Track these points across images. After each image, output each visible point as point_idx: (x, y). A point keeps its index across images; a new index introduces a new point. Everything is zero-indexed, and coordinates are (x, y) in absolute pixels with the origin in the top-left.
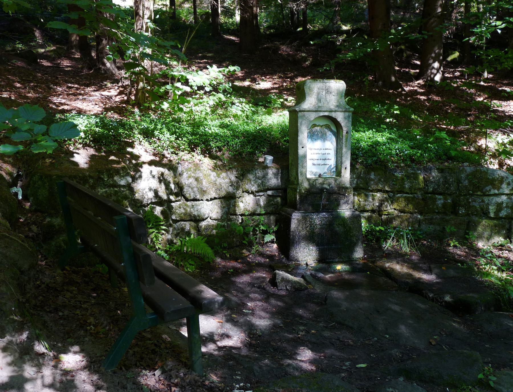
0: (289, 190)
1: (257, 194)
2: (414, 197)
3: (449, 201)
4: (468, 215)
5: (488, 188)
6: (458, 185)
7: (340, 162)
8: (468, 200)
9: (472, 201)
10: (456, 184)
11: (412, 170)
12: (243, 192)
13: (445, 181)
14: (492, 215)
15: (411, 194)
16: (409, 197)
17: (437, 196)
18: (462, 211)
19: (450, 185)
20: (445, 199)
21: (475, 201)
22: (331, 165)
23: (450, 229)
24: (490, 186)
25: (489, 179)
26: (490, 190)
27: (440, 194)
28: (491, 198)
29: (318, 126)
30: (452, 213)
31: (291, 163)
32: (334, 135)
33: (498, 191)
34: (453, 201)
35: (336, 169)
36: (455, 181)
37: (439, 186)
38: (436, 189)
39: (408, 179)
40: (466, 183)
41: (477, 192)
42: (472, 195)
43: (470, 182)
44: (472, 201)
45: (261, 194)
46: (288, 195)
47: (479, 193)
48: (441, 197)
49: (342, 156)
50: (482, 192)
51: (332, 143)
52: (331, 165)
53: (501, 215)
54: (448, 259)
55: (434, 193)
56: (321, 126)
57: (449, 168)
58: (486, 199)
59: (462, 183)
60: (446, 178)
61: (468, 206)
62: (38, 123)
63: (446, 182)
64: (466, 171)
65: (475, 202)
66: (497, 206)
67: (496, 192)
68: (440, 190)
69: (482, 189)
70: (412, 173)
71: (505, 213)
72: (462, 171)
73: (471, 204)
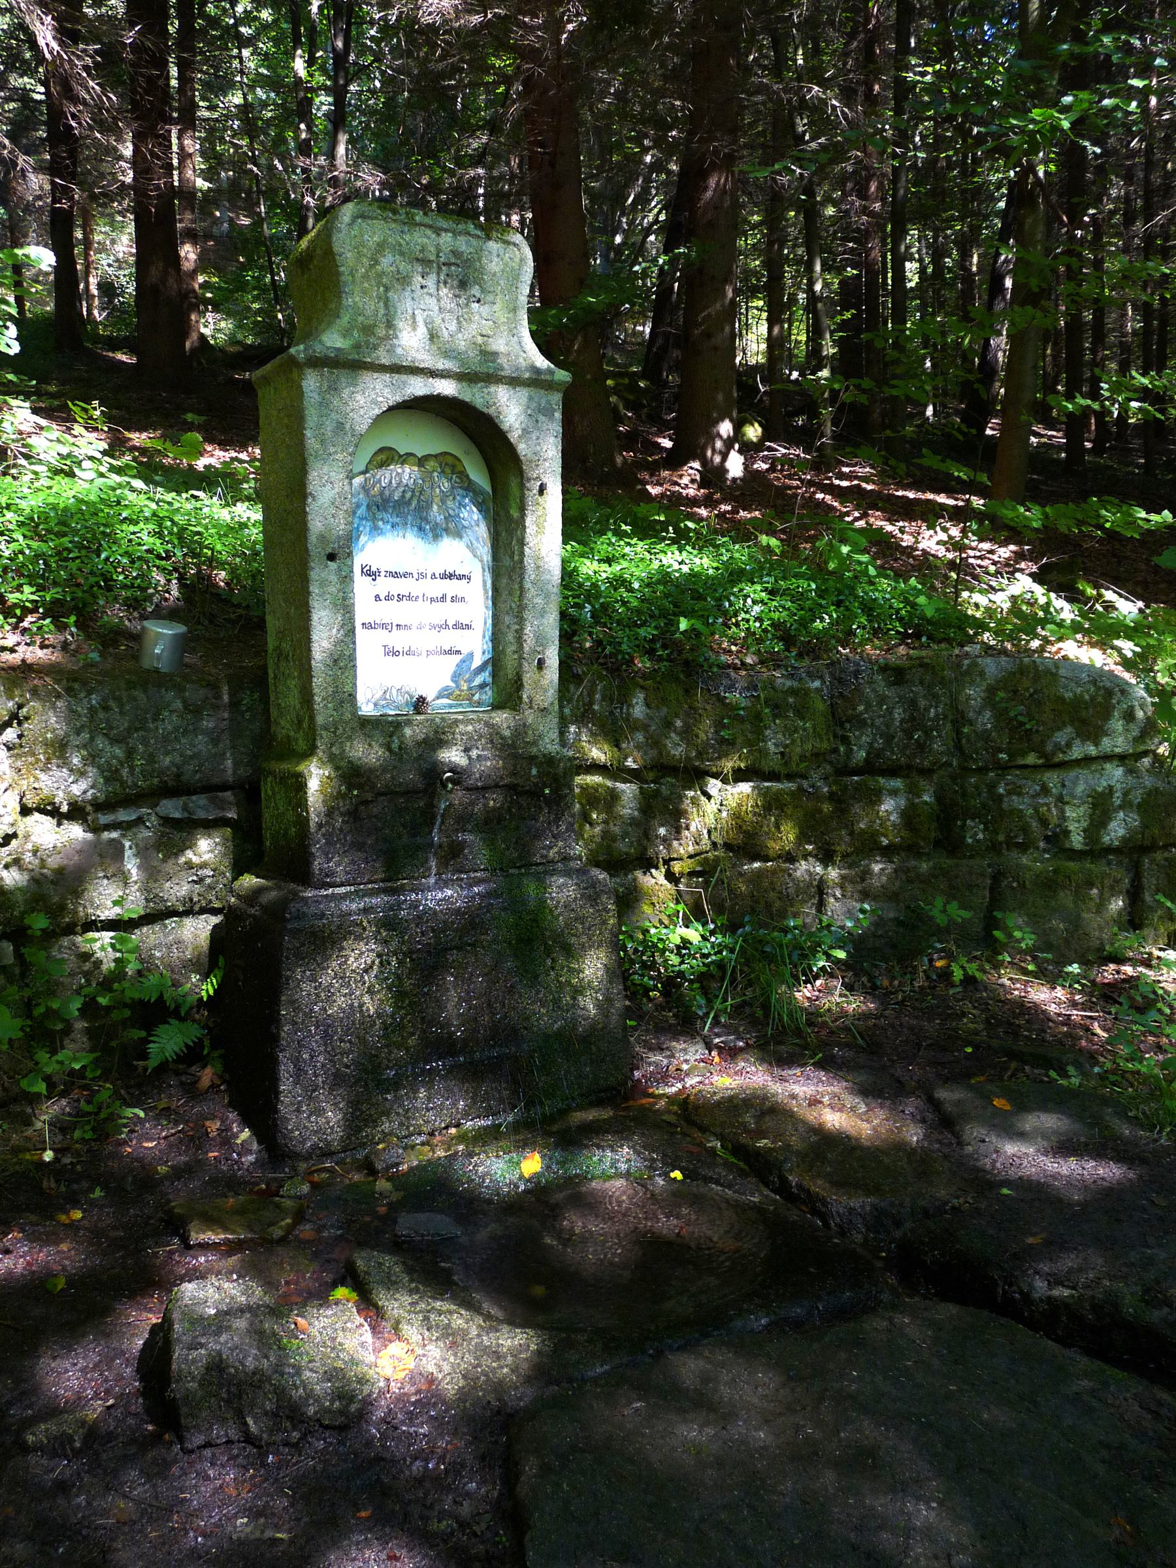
0: (267, 788)
1: (104, 819)
2: (801, 789)
3: (926, 798)
4: (994, 848)
5: (1061, 737)
6: (958, 732)
7: (510, 637)
8: (992, 787)
9: (1009, 793)
10: (949, 726)
11: (791, 676)
12: (25, 811)
13: (912, 719)
14: (1077, 841)
15: (790, 777)
16: (780, 793)
17: (882, 780)
18: (975, 833)
19: (927, 733)
20: (913, 791)
21: (1016, 791)
22: (471, 655)
23: (944, 911)
24: (1069, 729)
25: (1063, 699)
26: (1069, 745)
27: (893, 772)
28: (1073, 774)
29: (404, 459)
30: (937, 844)
31: (278, 648)
32: (481, 507)
33: (1096, 745)
34: (939, 798)
35: (494, 675)
36: (946, 717)
37: (889, 738)
38: (879, 754)
39: (775, 716)
40: (986, 720)
41: (1024, 754)
42: (1004, 768)
43: (1000, 715)
44: (1009, 793)
45: (123, 815)
46: (267, 815)
47: (1031, 759)
48: (897, 783)
49: (522, 608)
50: (1042, 754)
51: (471, 547)
52: (471, 655)
53: (1106, 839)
54: (976, 1047)
55: (870, 768)
56: (421, 462)
57: (922, 665)
58: (1052, 779)
59: (971, 723)
60: (913, 703)
61: (994, 813)
62: (50, 810)
63: (914, 721)
64: (982, 674)
65: (1019, 794)
66: (1094, 806)
67: (1092, 750)
68: (895, 756)
69: (1043, 742)
70: (793, 691)
71: (1121, 832)
72: (968, 673)
73: (1005, 806)
